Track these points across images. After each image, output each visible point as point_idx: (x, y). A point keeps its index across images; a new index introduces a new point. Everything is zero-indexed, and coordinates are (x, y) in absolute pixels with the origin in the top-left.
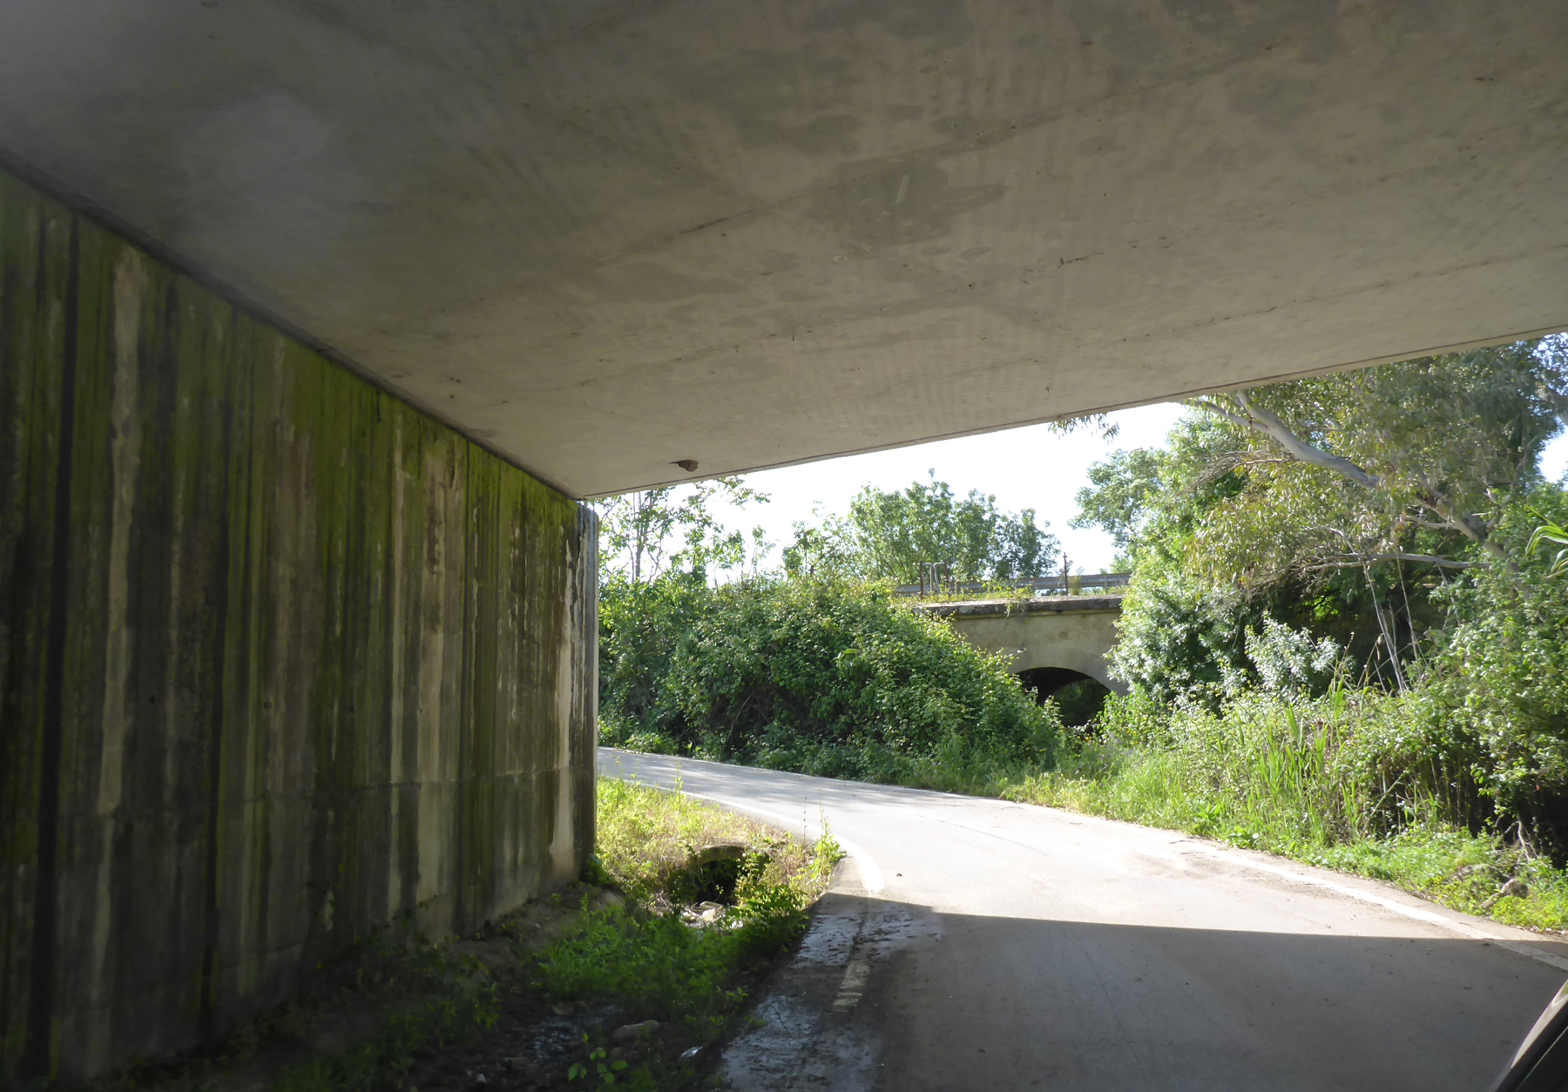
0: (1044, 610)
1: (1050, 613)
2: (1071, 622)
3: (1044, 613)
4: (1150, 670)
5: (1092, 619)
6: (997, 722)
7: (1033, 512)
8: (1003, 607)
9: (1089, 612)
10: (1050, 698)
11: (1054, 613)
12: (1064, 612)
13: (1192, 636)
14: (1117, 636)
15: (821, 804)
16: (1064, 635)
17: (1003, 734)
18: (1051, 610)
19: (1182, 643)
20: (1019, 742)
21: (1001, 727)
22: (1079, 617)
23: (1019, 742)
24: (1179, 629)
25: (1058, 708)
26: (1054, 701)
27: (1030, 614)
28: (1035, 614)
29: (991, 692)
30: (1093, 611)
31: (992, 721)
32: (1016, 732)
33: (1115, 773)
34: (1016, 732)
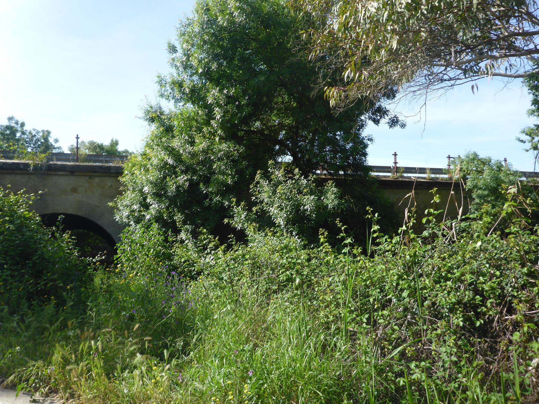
0: (61, 171)
1: (65, 173)
2: (81, 181)
3: (60, 173)
4: (153, 213)
5: (97, 180)
6: (12, 253)
7: (49, 133)
8: (27, 165)
9: (95, 174)
10: (68, 233)
11: (68, 173)
12: (76, 174)
13: (193, 185)
14: (121, 188)
15: (397, 170)
16: (74, 190)
17: (19, 267)
18: (66, 171)
19: (184, 191)
20: (38, 274)
21: (17, 258)
22: (87, 178)
23: (38, 274)
24: (182, 179)
25: (75, 241)
26: (71, 235)
27: (49, 173)
28: (53, 173)
29: (7, 218)
30: (98, 174)
31: (7, 251)
32: (35, 264)
33: (207, 316)
34: (35, 264)
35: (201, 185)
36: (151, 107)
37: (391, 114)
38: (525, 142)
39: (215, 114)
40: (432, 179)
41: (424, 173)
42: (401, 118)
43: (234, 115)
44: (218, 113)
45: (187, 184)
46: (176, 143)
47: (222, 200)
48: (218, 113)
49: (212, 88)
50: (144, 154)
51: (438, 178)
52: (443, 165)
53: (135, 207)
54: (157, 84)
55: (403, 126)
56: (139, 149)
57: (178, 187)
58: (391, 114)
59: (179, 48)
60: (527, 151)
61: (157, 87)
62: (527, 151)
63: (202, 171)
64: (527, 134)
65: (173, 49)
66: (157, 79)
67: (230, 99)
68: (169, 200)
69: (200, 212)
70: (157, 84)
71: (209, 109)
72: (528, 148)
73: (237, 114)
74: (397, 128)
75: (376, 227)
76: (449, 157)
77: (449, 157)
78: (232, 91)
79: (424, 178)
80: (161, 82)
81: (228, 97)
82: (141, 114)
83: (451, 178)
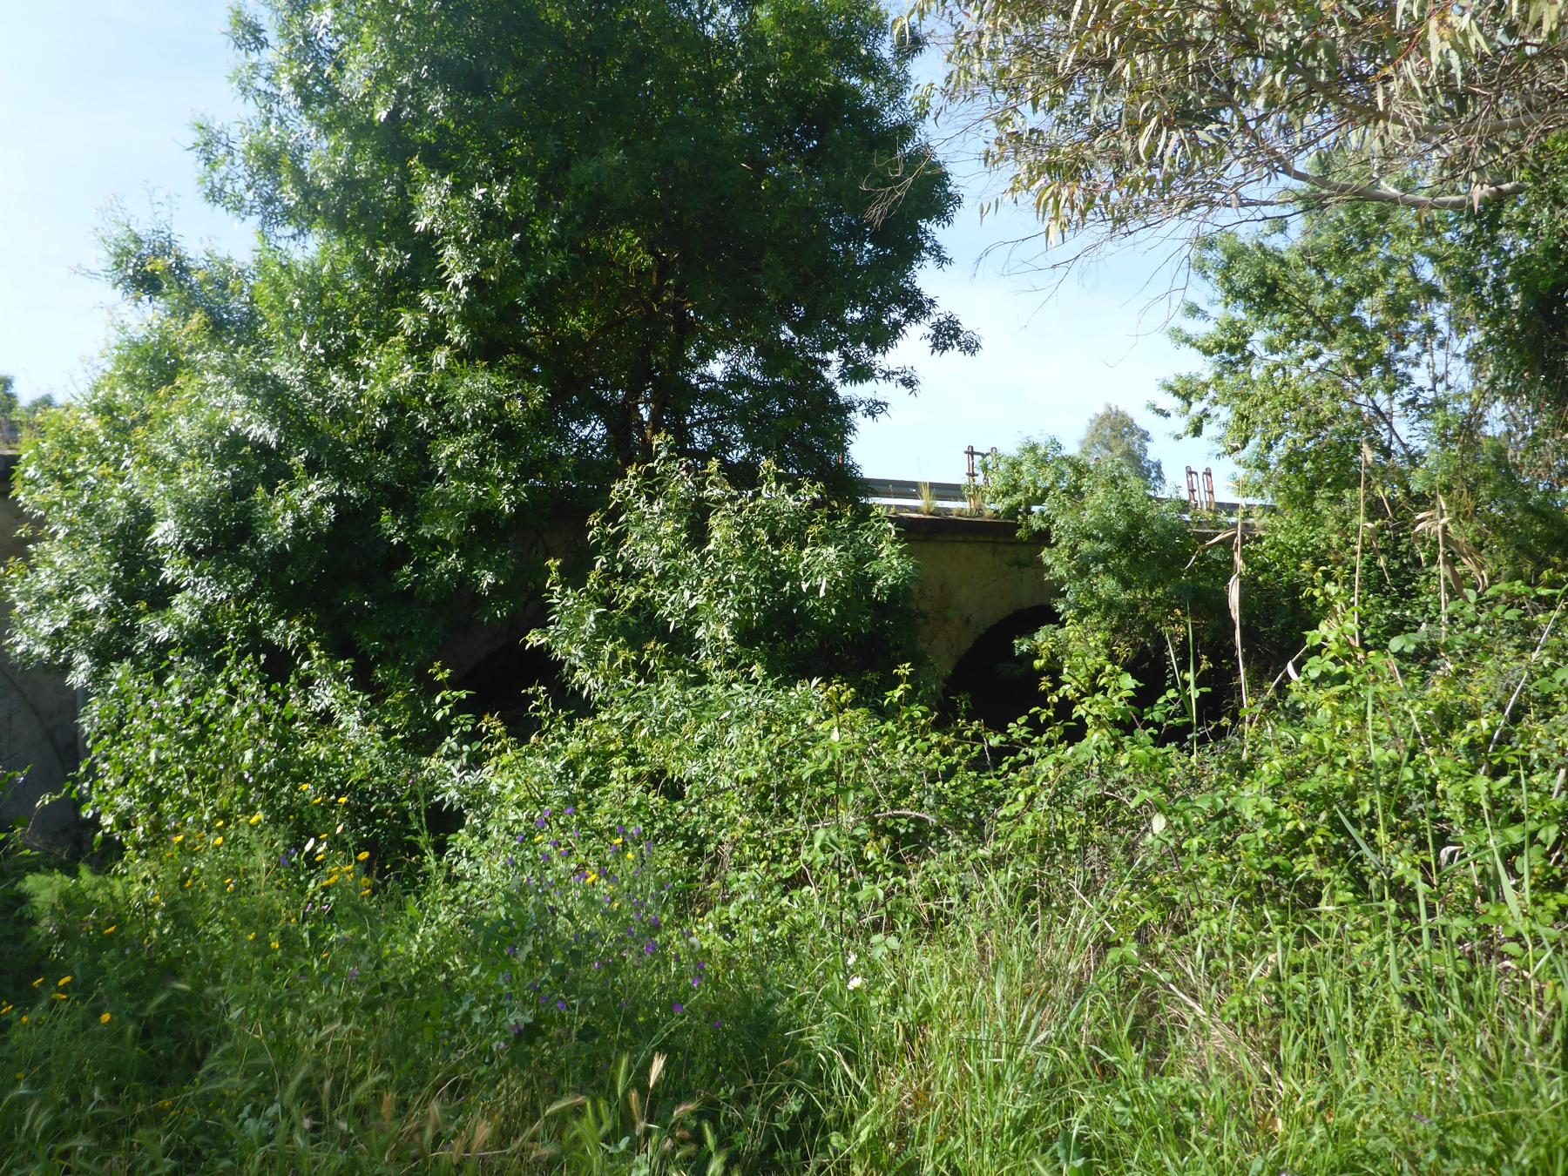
13: (353, 519)
14: (23, 531)
35: (385, 517)
36: (138, 240)
37: (939, 313)
38: (1168, 415)
39: (444, 268)
40: (938, 511)
41: (914, 496)
42: (965, 326)
43: (510, 278)
44: (456, 268)
45: (329, 511)
46: (287, 370)
47: (469, 567)
48: (456, 268)
49: (428, 179)
50: (107, 410)
51: (948, 510)
52: (958, 477)
53: (91, 600)
54: (194, 153)
55: (971, 347)
56: (84, 387)
57: (299, 523)
58: (939, 313)
59: (271, 35)
60: (1178, 437)
61: (192, 165)
62: (1178, 437)
63: (385, 468)
64: (1176, 393)
65: (251, 35)
66: (195, 137)
67: (491, 222)
68: (254, 569)
69: (371, 612)
70: (194, 153)
71: (425, 248)
72: (1181, 431)
73: (522, 274)
74: (954, 354)
75: (1408, 613)
76: (971, 453)
77: (971, 453)
78: (502, 193)
79: (916, 510)
80: (209, 145)
81: (487, 212)
82: (101, 259)
83: (980, 511)
